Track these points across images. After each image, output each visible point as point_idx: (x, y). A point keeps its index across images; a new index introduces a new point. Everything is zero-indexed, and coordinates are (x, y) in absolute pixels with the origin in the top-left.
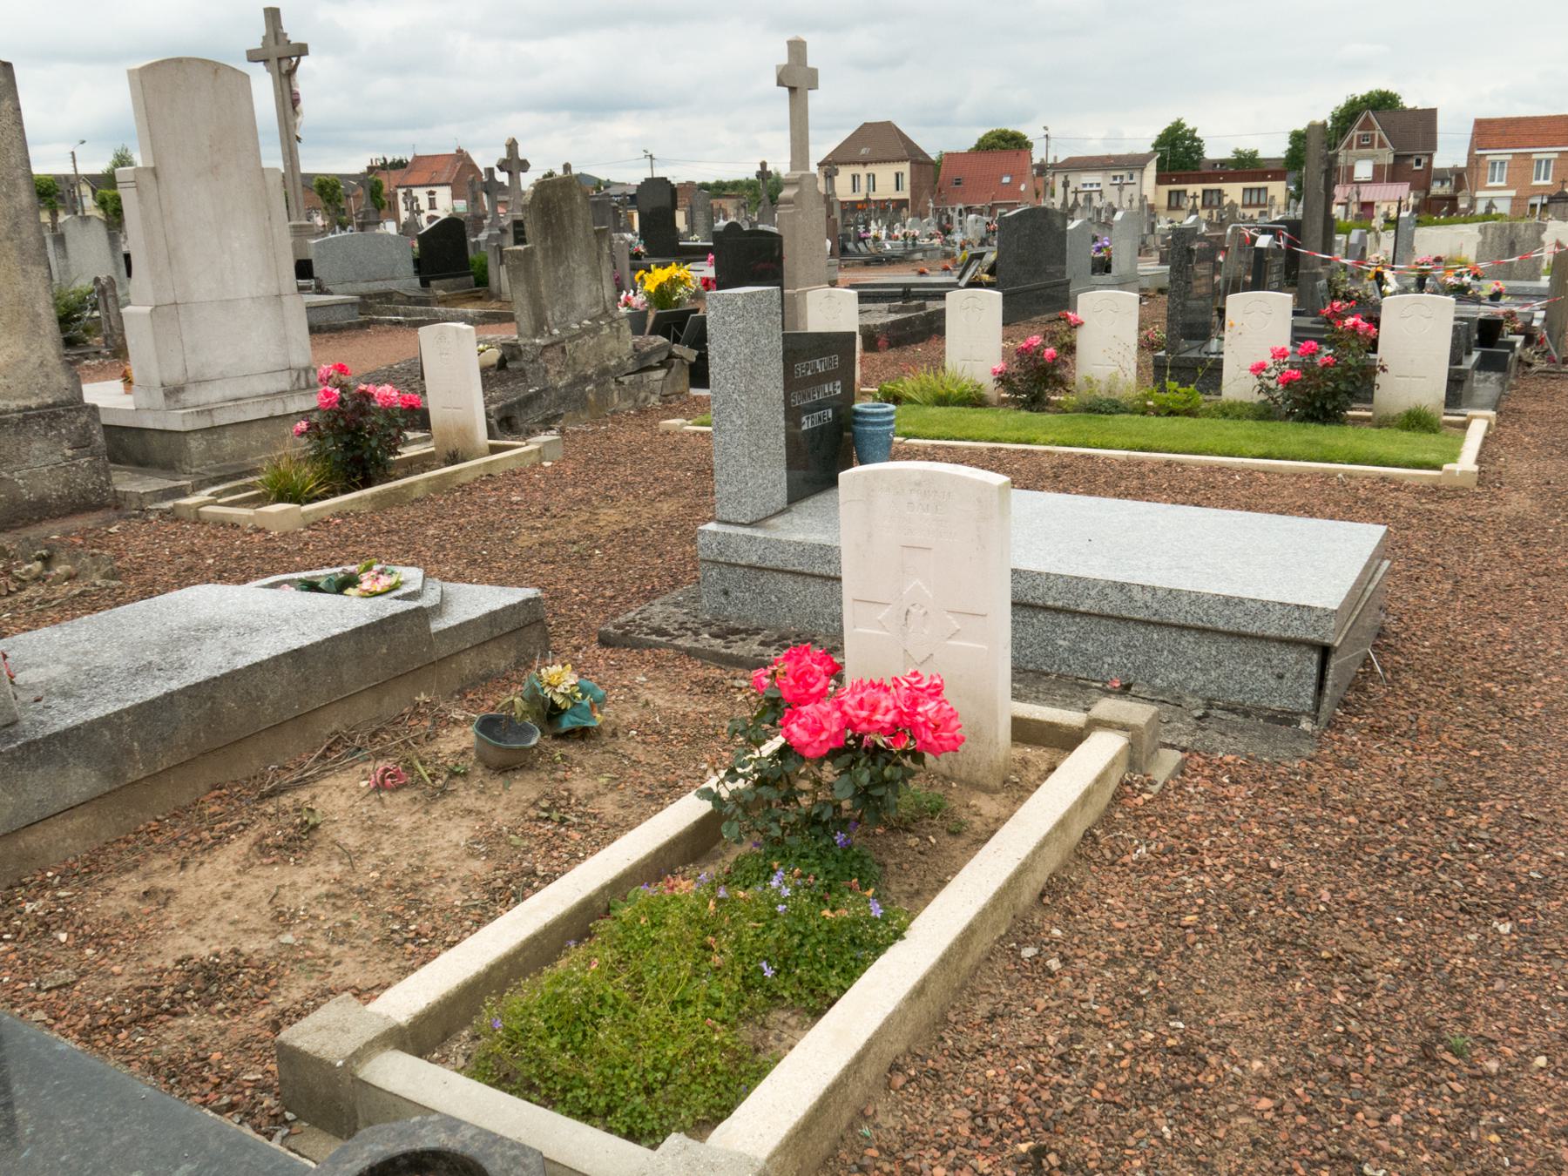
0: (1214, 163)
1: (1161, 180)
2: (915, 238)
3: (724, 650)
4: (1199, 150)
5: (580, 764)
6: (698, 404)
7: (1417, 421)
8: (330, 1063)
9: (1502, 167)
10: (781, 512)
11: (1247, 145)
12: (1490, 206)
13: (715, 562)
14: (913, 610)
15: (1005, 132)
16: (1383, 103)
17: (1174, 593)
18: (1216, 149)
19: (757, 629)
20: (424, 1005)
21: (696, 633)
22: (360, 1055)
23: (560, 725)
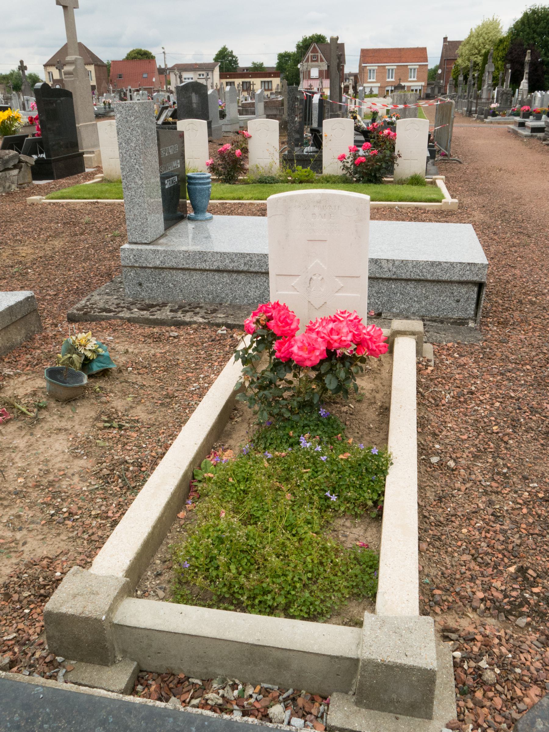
0: (243, 69)
1: (222, 77)
2: (109, 104)
3: (151, 317)
4: (236, 62)
5: (111, 392)
6: (40, 188)
7: (416, 181)
8: (96, 619)
9: (374, 72)
10: (162, 236)
11: (258, 61)
12: (371, 91)
13: (133, 267)
14: (314, 278)
15: (141, 50)
16: (319, 39)
17: (405, 262)
18: (244, 62)
19: (163, 303)
20: (129, 563)
21: (129, 309)
22: (112, 609)
23: (92, 369)
